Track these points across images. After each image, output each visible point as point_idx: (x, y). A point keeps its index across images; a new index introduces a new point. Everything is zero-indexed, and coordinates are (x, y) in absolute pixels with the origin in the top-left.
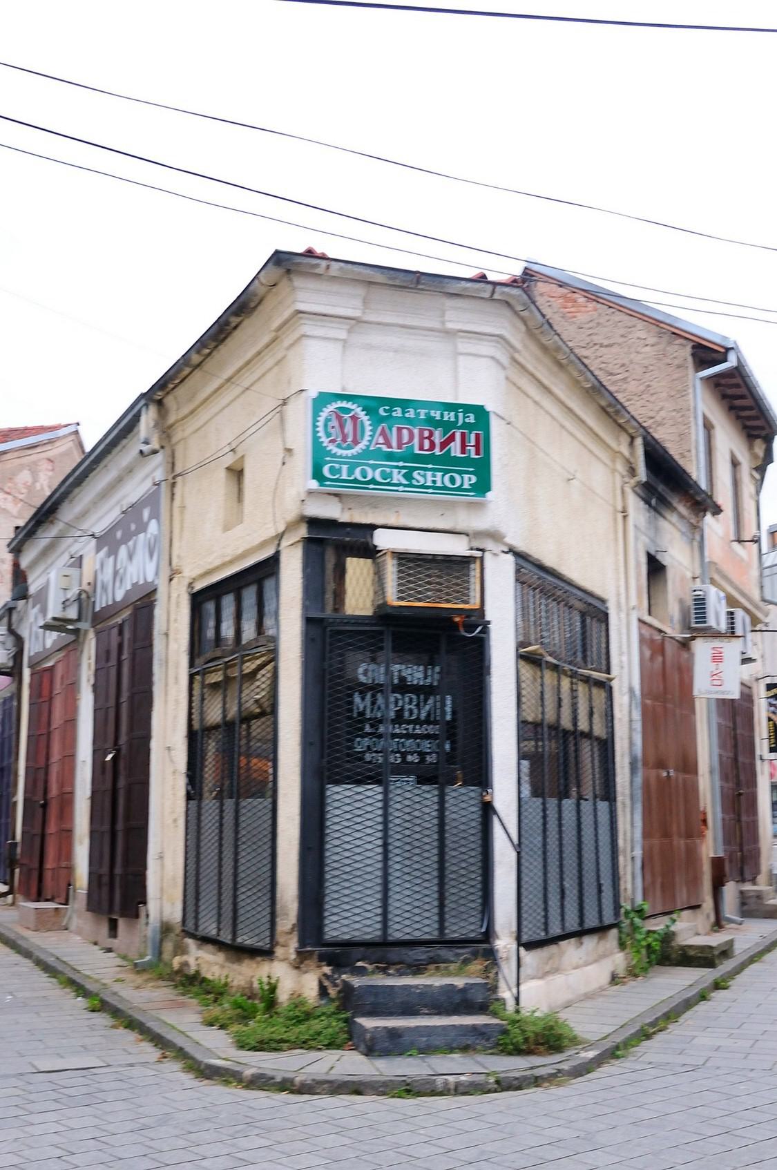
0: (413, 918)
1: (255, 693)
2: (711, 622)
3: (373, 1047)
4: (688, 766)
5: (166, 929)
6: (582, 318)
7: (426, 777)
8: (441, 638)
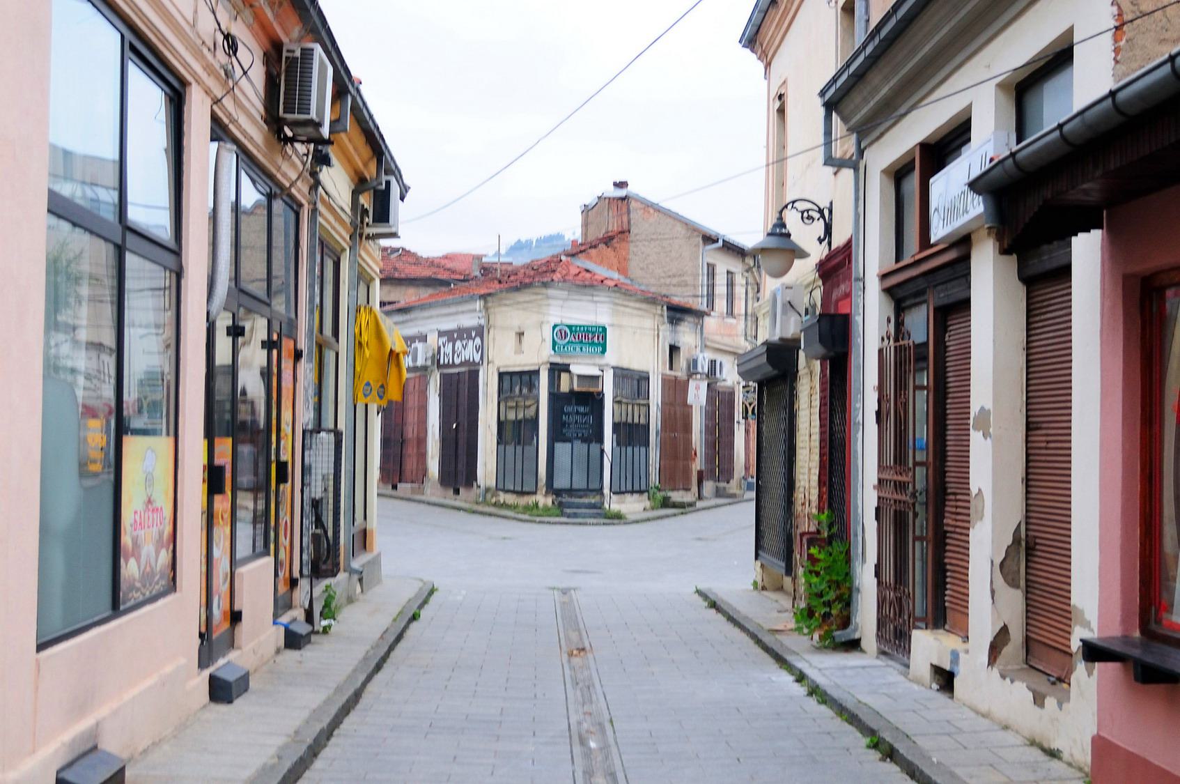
0: (579, 483)
1: (530, 413)
2: (700, 369)
3: (569, 516)
4: (687, 428)
5: (487, 490)
6: (652, 220)
7: (585, 440)
8: (590, 400)
